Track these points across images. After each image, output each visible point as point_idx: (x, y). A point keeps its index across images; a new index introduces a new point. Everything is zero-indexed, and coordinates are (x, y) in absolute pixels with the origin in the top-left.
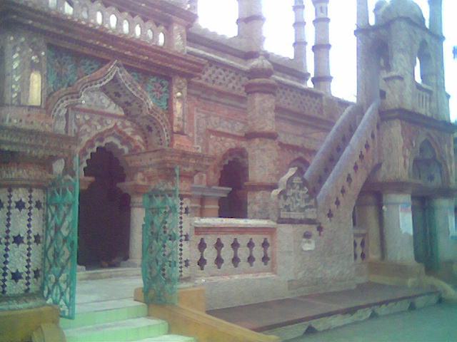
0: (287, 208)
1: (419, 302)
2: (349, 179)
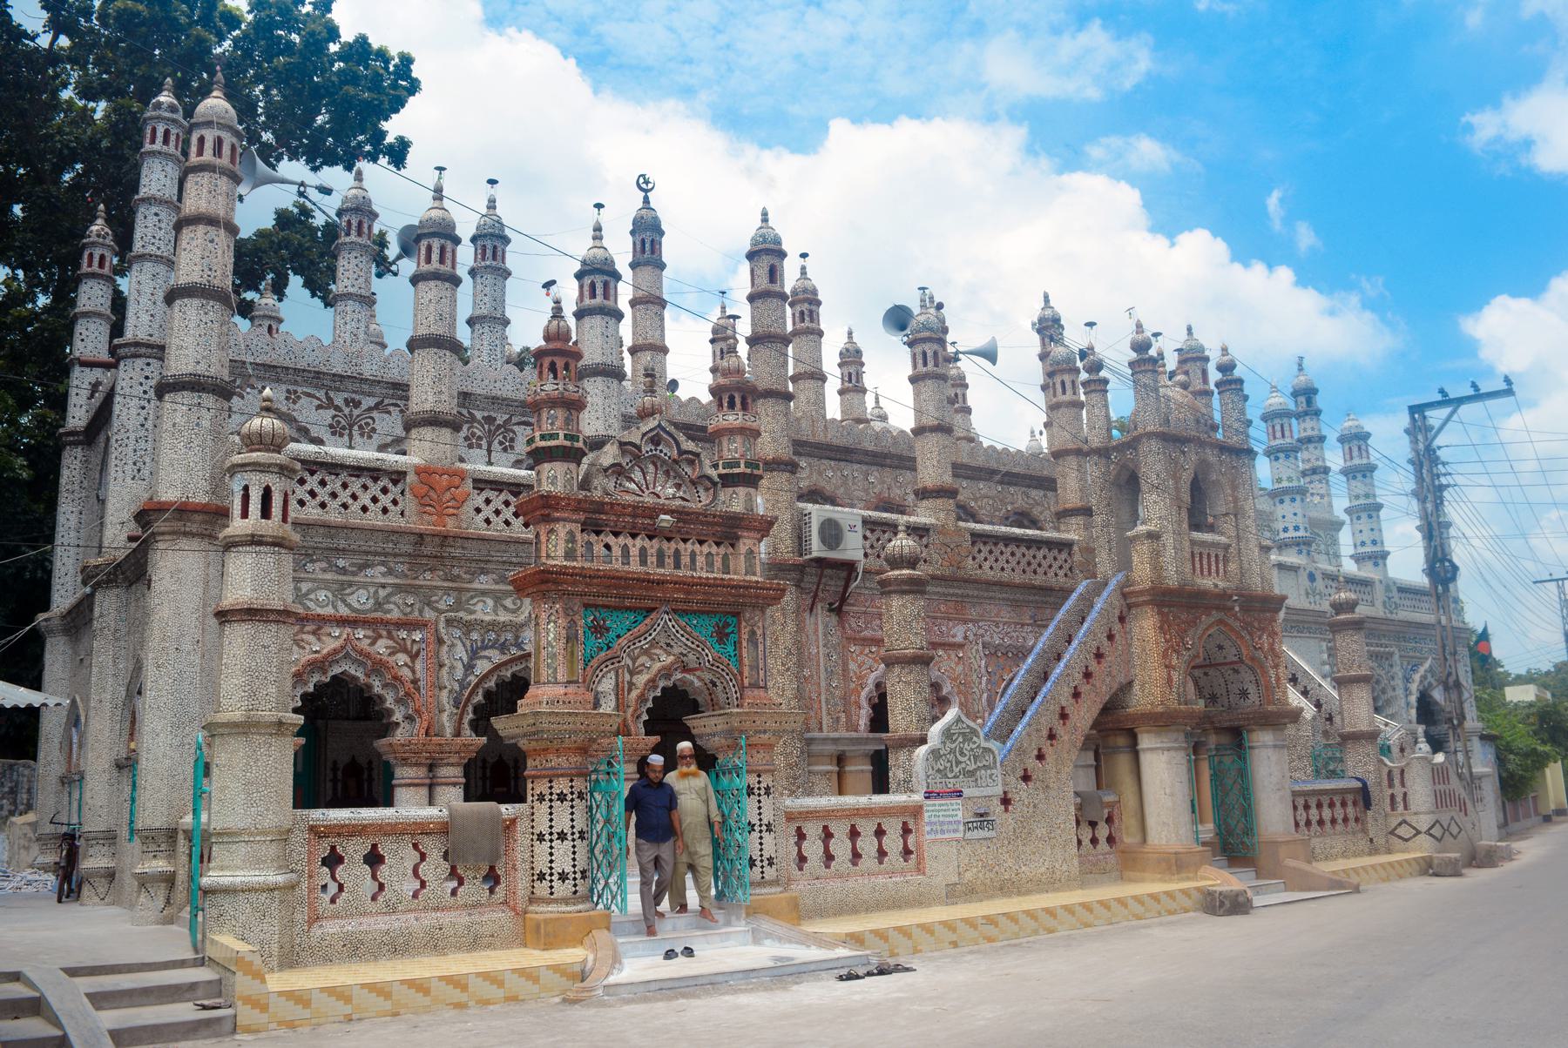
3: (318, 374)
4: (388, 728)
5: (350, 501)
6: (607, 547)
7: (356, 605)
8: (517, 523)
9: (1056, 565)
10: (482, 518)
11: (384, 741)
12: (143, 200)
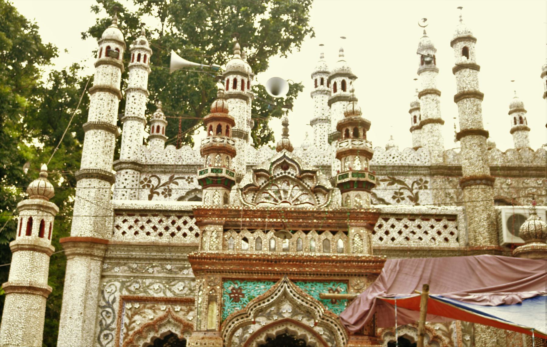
7: (177, 292)
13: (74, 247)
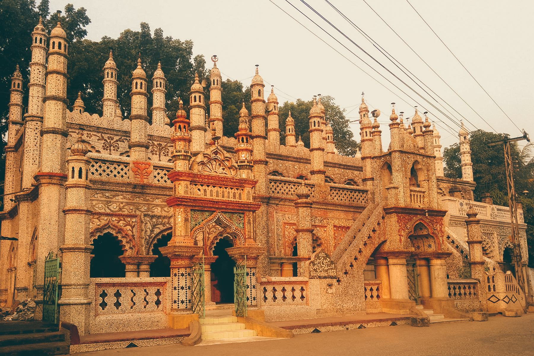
0: (315, 270)
1: (398, 323)
2: (360, 251)
3: (98, 128)
4: (122, 252)
5: (110, 173)
6: (199, 190)
7: (112, 209)
8: (169, 182)
9: (361, 199)
10: (156, 179)
11: (121, 256)
12: (33, 64)
13: (50, 179)
